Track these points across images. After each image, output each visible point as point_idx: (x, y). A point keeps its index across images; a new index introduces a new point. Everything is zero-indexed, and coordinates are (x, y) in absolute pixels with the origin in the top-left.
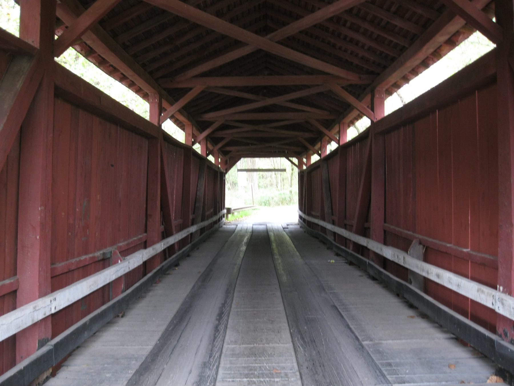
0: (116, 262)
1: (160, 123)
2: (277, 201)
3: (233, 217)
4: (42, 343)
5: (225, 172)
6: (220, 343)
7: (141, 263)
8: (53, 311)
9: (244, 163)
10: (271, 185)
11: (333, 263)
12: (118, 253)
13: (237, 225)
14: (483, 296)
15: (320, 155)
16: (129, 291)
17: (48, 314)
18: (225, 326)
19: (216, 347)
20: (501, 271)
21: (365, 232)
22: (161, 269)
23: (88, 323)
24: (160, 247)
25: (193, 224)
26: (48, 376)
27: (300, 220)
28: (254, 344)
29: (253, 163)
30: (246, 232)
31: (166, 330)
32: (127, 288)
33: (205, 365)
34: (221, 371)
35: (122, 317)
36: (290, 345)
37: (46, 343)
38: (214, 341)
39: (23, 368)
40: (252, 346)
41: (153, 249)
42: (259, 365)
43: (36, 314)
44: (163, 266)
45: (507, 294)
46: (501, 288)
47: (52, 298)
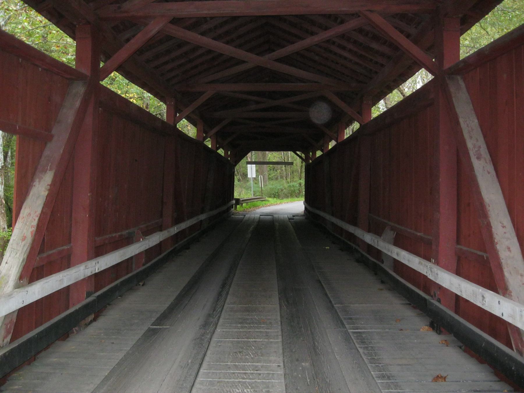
0: (138, 241)
1: (176, 123)
2: (286, 193)
3: (241, 208)
4: (89, 295)
5: (234, 164)
6: (222, 303)
7: (158, 242)
8: (97, 271)
9: (252, 156)
10: (282, 177)
11: (327, 249)
12: (141, 232)
13: (245, 215)
14: (421, 267)
15: (322, 151)
16: (149, 265)
17: (94, 273)
18: (227, 292)
19: (219, 305)
20: (434, 247)
21: (354, 222)
22: (174, 249)
23: (119, 285)
24: (174, 230)
25: (202, 213)
26: (92, 320)
27: (306, 212)
28: (249, 305)
29: (264, 156)
30: (253, 222)
31: (179, 295)
32: (147, 262)
33: (209, 315)
34: (221, 320)
35: (143, 285)
36: (278, 306)
37: (91, 295)
38: (217, 301)
39: (78, 308)
40: (247, 306)
41: (168, 232)
42: (251, 317)
43: (86, 270)
44: (176, 248)
45: (436, 265)
46: (433, 260)
47: (97, 261)
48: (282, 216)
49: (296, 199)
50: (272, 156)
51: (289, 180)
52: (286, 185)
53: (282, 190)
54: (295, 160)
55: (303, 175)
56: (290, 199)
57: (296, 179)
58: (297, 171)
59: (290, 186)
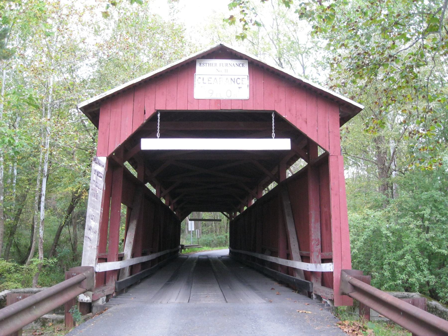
9: (194, 215)
10: (212, 232)
21: (254, 251)
29: (199, 215)
32: (152, 266)
48: (214, 257)
49: (223, 247)
50: (205, 215)
51: (218, 233)
52: (215, 237)
53: (213, 241)
54: (223, 218)
55: (228, 230)
56: (218, 248)
57: (224, 232)
58: (224, 227)
59: (219, 238)
